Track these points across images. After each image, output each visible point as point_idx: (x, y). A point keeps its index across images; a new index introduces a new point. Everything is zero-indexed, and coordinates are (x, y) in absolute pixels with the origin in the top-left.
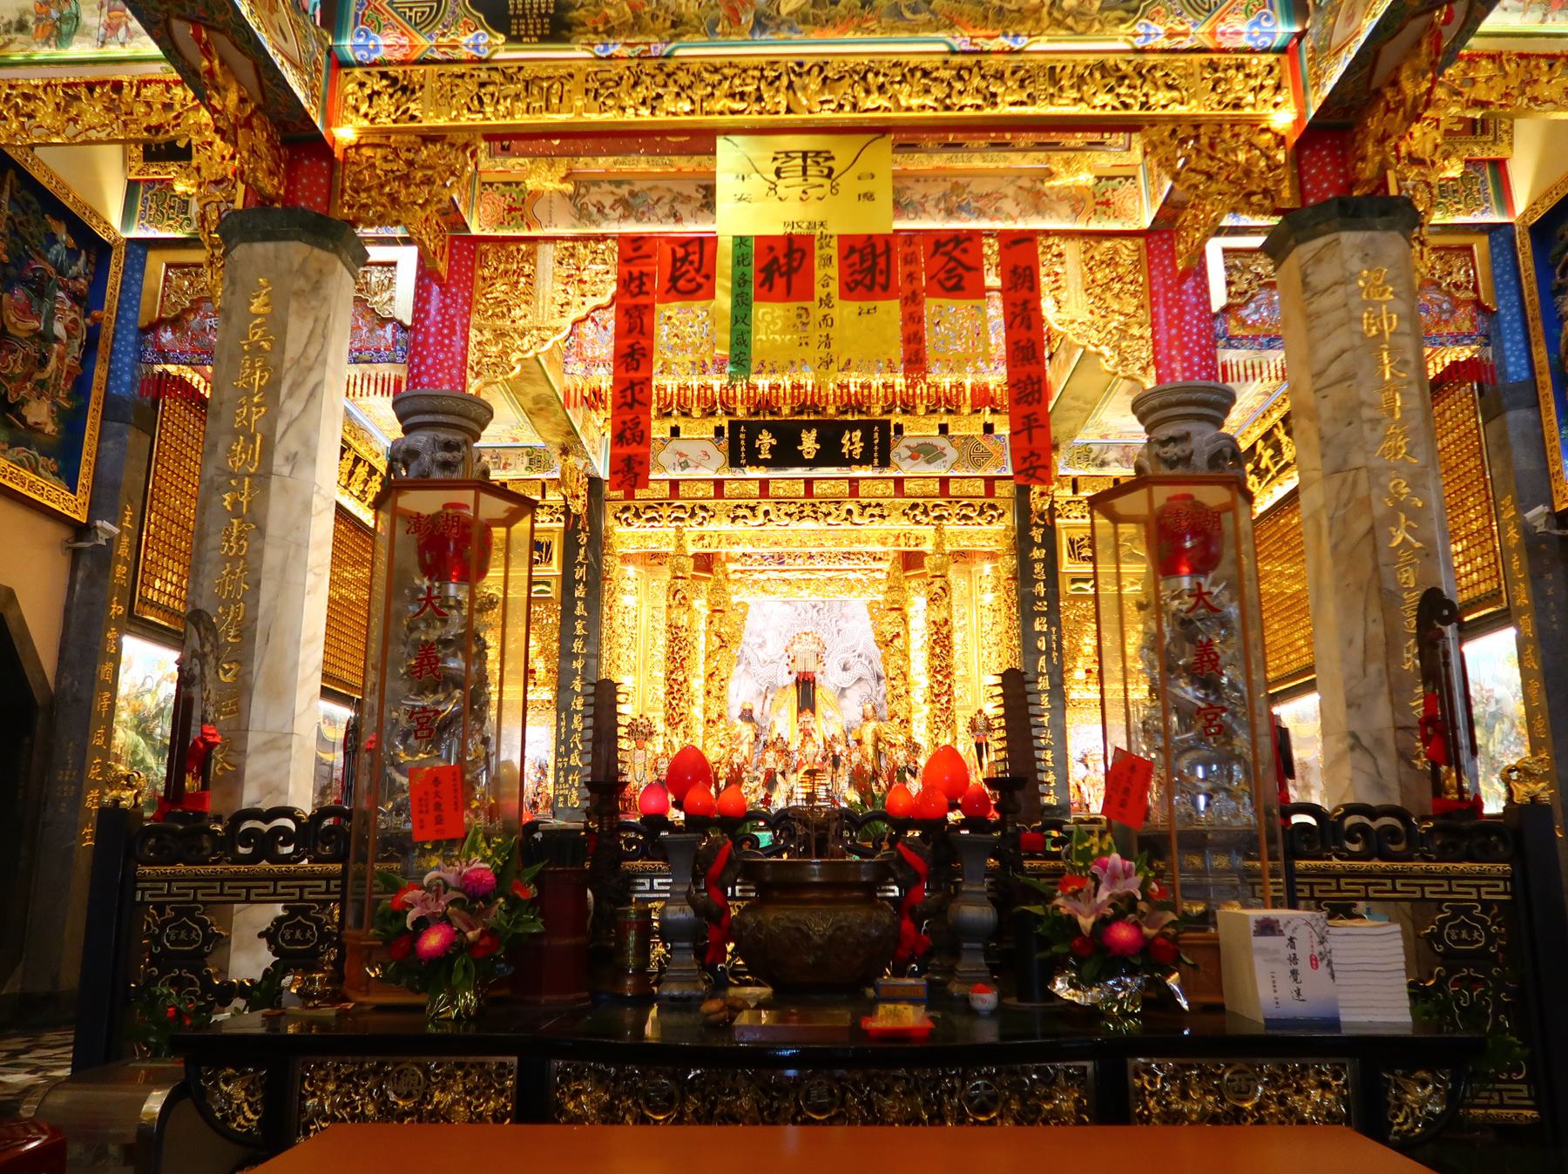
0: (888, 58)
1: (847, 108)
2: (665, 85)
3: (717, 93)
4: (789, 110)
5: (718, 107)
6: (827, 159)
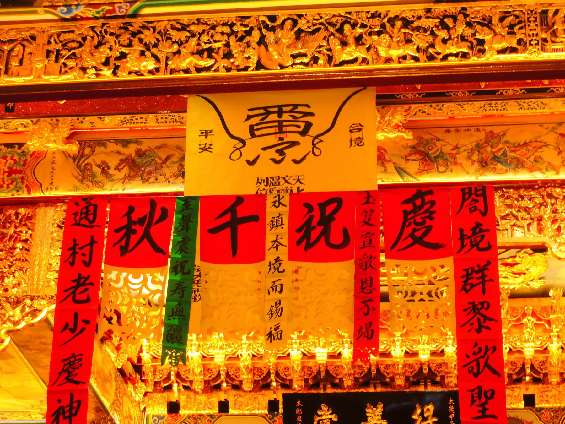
0: (366, 9)
1: (321, 62)
2: (130, 45)
3: (184, 51)
4: (259, 66)
5: (184, 65)
6: (306, 114)
